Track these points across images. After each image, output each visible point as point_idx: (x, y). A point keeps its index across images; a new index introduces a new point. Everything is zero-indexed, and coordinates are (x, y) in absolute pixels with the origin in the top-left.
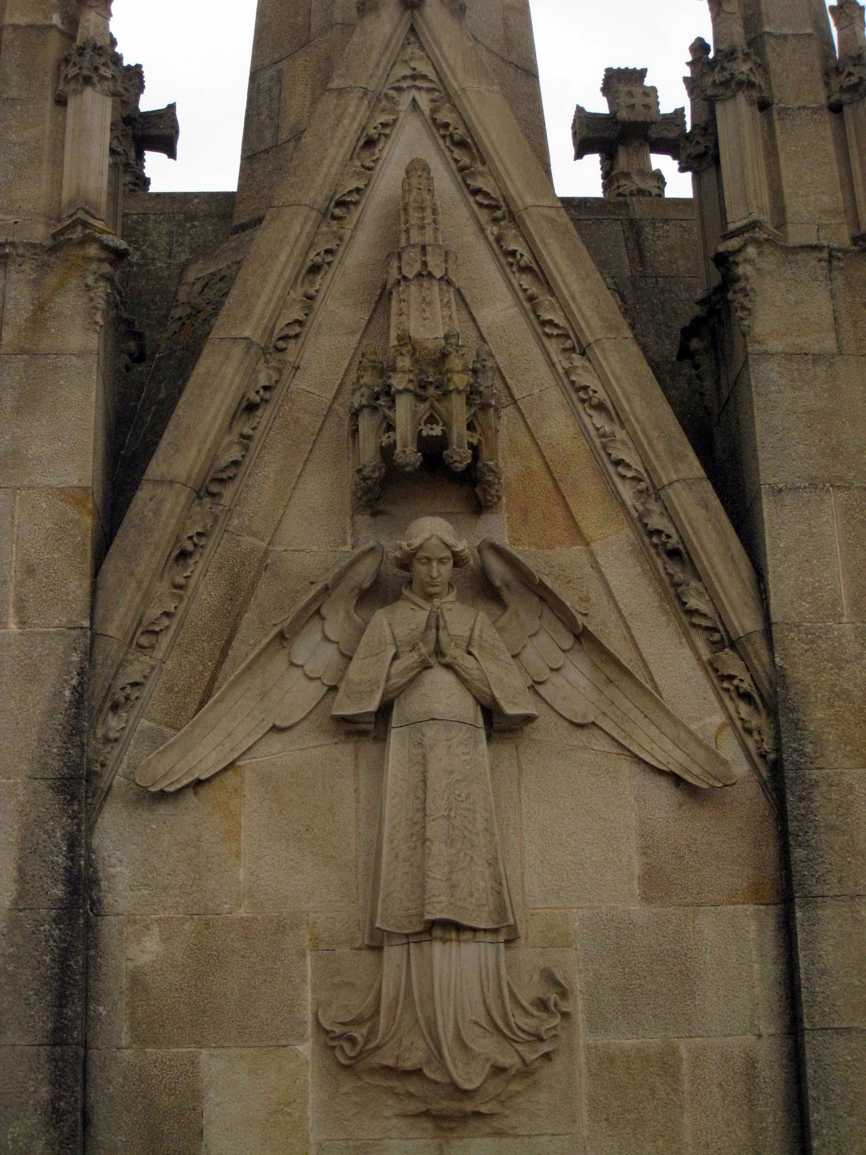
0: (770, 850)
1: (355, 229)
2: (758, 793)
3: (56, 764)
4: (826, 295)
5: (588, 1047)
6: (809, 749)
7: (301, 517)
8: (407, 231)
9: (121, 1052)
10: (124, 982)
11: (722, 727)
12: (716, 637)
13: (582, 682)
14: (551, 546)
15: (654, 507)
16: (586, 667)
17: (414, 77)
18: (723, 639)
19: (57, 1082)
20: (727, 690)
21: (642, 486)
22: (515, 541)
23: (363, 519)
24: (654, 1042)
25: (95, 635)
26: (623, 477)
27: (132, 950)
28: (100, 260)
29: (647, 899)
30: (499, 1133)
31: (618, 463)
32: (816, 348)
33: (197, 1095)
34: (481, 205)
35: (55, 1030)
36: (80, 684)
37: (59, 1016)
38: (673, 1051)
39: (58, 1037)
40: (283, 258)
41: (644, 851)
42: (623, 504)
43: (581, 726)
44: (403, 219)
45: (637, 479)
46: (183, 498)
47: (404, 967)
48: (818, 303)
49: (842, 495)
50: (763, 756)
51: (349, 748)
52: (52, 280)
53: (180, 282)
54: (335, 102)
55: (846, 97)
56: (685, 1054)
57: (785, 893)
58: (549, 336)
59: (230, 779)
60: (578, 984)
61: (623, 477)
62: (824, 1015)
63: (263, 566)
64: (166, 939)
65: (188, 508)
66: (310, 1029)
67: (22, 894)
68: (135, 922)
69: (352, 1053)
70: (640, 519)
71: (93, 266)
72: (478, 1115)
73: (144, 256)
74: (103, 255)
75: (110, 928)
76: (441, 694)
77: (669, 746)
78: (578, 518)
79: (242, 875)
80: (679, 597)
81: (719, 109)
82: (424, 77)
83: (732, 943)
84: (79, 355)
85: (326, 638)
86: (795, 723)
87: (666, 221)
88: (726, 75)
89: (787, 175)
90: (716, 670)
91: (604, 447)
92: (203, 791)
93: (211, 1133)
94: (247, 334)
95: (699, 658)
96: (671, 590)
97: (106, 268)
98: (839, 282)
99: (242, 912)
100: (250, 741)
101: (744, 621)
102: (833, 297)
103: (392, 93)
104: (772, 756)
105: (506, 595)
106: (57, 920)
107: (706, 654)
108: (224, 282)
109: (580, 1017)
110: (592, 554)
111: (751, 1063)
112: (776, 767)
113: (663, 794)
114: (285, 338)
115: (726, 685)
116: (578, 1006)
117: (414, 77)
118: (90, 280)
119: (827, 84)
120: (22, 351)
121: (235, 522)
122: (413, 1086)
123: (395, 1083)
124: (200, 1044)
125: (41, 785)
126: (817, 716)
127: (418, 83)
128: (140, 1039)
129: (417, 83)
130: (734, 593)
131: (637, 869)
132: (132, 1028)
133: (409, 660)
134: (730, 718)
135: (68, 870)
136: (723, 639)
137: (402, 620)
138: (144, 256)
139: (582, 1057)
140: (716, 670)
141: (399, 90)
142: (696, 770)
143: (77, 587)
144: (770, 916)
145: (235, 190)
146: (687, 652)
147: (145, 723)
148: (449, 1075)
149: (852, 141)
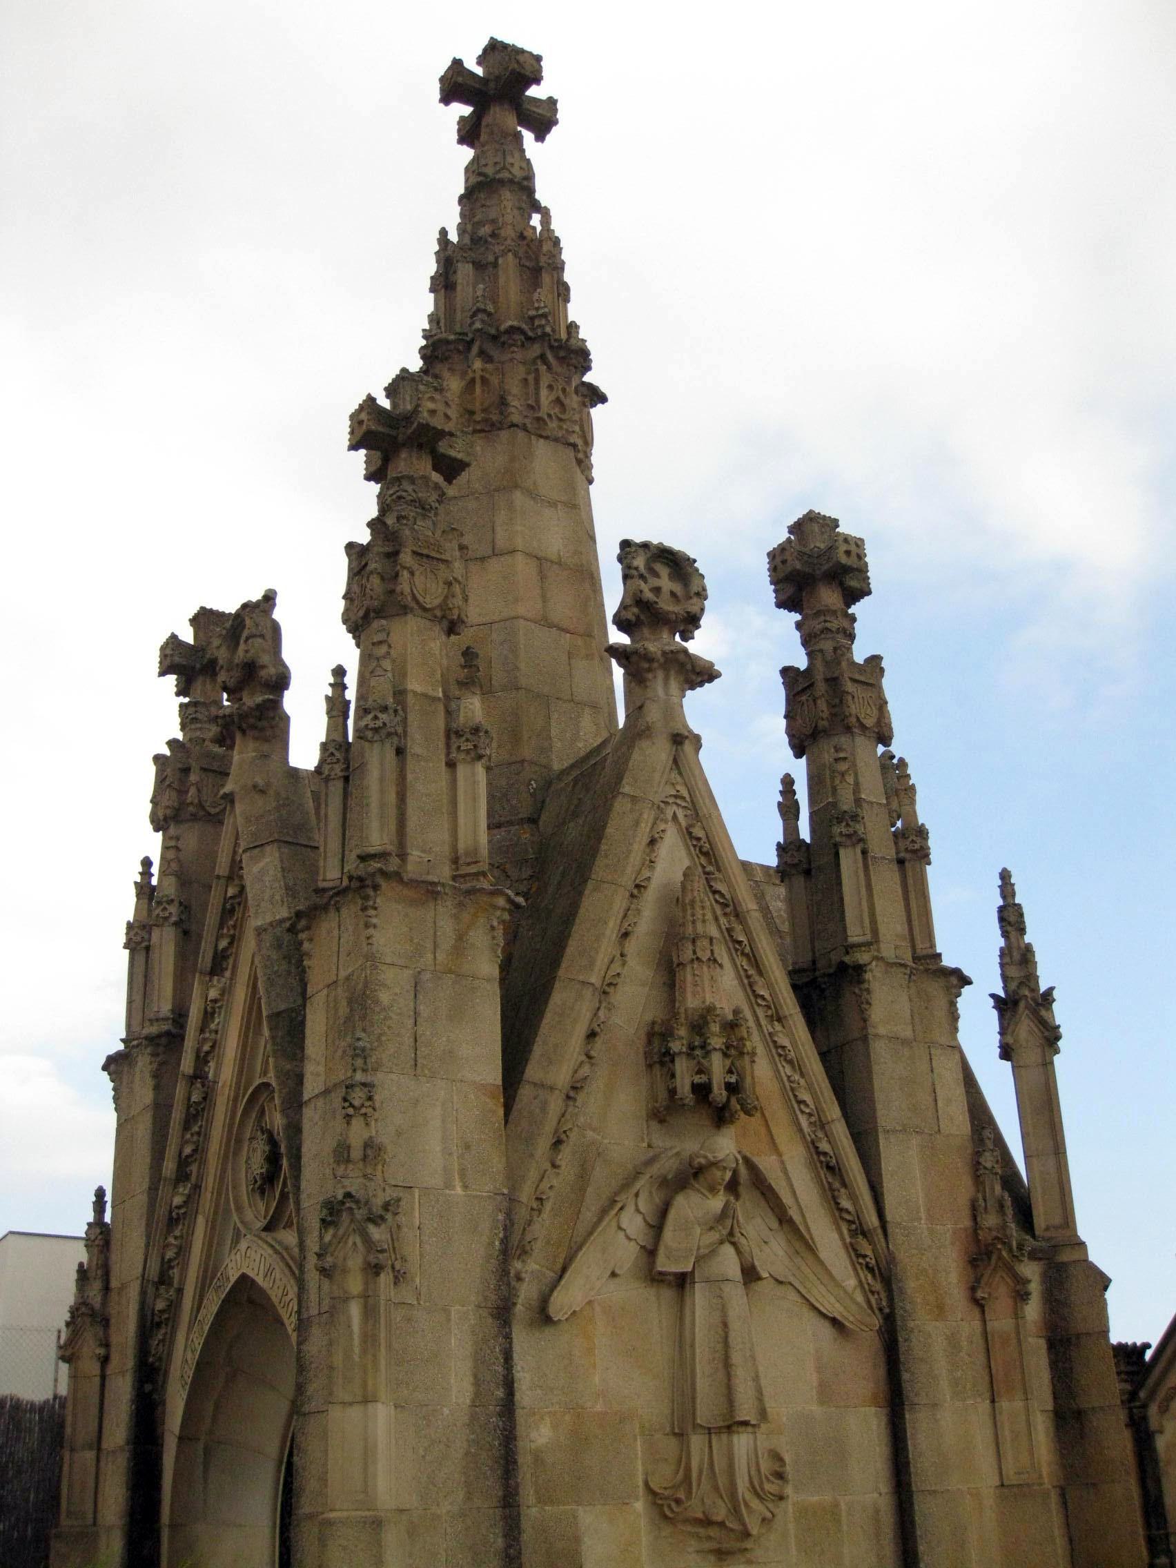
3: (493, 1297)
6: (908, 1307)
7: (615, 1120)
8: (694, 922)
9: (531, 1511)
10: (529, 1458)
12: (853, 1227)
13: (781, 1253)
15: (820, 1134)
16: (783, 1243)
17: (676, 797)
18: (859, 1230)
20: (860, 1264)
21: (813, 1119)
23: (654, 1124)
24: (828, 1498)
25: (512, 1200)
26: (802, 1112)
27: (534, 1435)
28: (504, 909)
29: (822, 1403)
30: (749, 1562)
31: (800, 1102)
32: (902, 1035)
33: (577, 1540)
34: (717, 901)
35: (505, 1497)
36: (506, 1237)
41: (819, 1369)
42: (801, 1130)
43: (781, 1283)
44: (689, 912)
45: (810, 1115)
47: (707, 1450)
50: (881, 1310)
51: (652, 1291)
52: (466, 916)
54: (629, 805)
55: (908, 856)
56: (843, 1507)
57: (895, 1401)
58: (759, 1005)
60: (787, 1458)
61: (802, 1112)
64: (555, 1427)
66: (641, 1490)
67: (477, 1394)
68: (534, 1414)
69: (666, 1507)
70: (813, 1142)
71: (498, 913)
74: (508, 907)
76: (728, 1263)
77: (832, 1300)
78: (776, 1137)
79: (597, 1379)
80: (834, 1198)
81: (842, 852)
82: (683, 798)
83: (866, 1429)
84: (488, 980)
86: (900, 1289)
88: (851, 830)
90: (855, 1250)
91: (792, 1089)
95: (842, 1239)
96: (829, 1193)
97: (506, 916)
101: (872, 1220)
103: (662, 805)
104: (887, 1311)
105: (742, 1189)
106: (500, 1415)
110: (782, 1162)
113: (826, 1330)
114: (610, 984)
115: (861, 1260)
117: (676, 797)
118: (495, 924)
119: (896, 843)
120: (450, 971)
121: (582, 1119)
122: (713, 1532)
123: (701, 1531)
124: (578, 1503)
125: (485, 1313)
127: (679, 801)
128: (541, 1501)
129: (679, 801)
132: (536, 1492)
133: (714, 1236)
134: (860, 1281)
136: (859, 1230)
140: (855, 1250)
141: (666, 803)
142: (851, 1319)
146: (836, 1236)
148: (744, 1525)
149: (911, 888)
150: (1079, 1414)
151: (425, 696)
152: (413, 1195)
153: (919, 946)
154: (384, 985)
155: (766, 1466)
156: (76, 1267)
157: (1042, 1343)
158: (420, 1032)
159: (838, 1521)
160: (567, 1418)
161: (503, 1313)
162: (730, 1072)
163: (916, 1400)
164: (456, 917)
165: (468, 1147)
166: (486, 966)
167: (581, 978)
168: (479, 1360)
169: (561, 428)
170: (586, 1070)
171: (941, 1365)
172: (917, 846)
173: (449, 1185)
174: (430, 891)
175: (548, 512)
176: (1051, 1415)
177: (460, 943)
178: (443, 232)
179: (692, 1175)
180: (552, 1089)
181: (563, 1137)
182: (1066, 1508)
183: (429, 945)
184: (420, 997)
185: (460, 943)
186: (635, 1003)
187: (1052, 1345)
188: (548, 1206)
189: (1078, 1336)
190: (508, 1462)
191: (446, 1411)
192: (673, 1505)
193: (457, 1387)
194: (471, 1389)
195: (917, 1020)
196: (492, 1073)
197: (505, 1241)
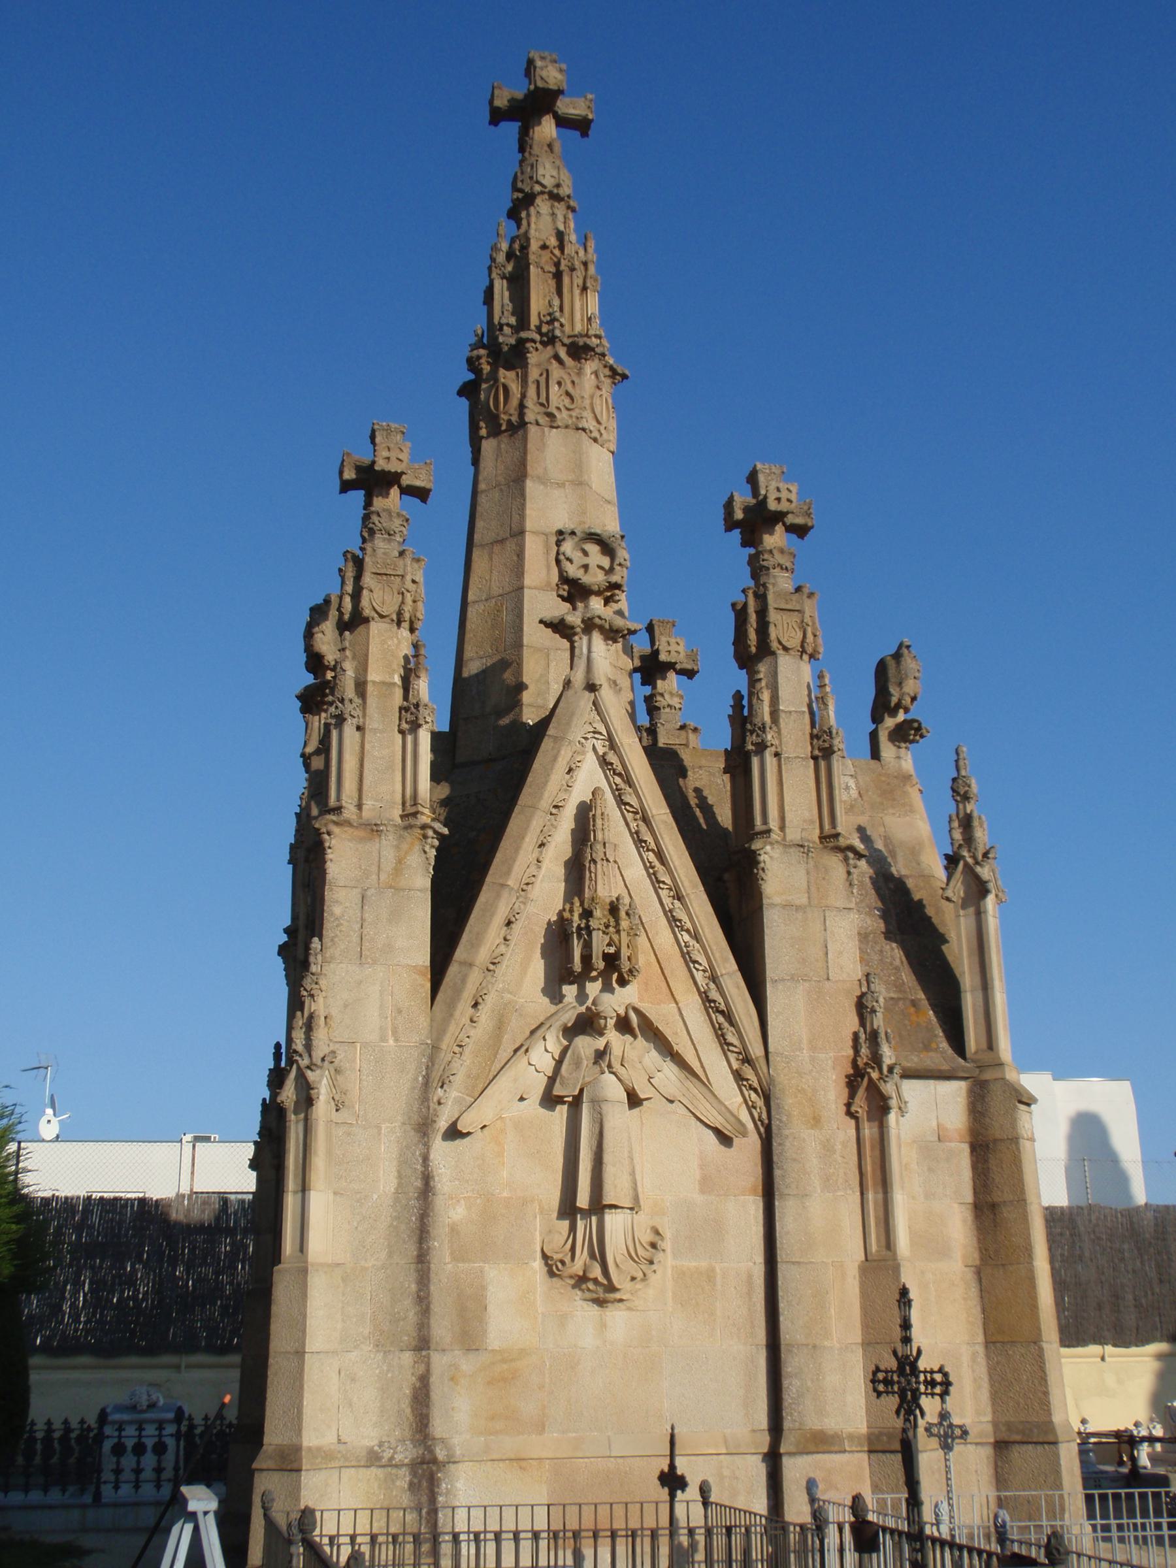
4: (804, 872)
5: (673, 1267)
6: (784, 1119)
11: (740, 1105)
13: (674, 1078)
14: (659, 1004)
15: (712, 986)
22: (641, 1000)
24: (704, 1264)
26: (697, 970)
27: (452, 1213)
29: (702, 1191)
30: (629, 1309)
32: (798, 902)
33: (483, 1288)
38: (713, 1270)
41: (702, 1167)
48: (799, 876)
49: (807, 984)
52: (405, 846)
56: (718, 1271)
60: (668, 1233)
61: (697, 970)
62: (787, 1254)
66: (539, 1255)
67: (400, 1185)
72: (621, 1300)
76: (612, 1089)
77: (716, 1114)
82: (600, 733)
84: (420, 891)
85: (547, 1051)
87: (700, 767)
93: (490, 1308)
99: (505, 1194)
101: (756, 1050)
102: (808, 873)
106: (418, 1199)
107: (735, 1065)
109: (669, 1250)
110: (679, 1009)
111: (750, 1276)
112: (768, 1128)
114: (527, 884)
116: (667, 1244)
117: (594, 732)
120: (391, 887)
125: (408, 1128)
128: (455, 1259)
130: (751, 1036)
131: (698, 1177)
132: (452, 1254)
137: (585, 1045)
139: (669, 1271)
141: (586, 739)
142: (730, 1128)
150: (993, 1207)
151: (384, 683)
153: (827, 826)
154: (337, 902)
155: (646, 1237)
156: (261, 1102)
157: (966, 1148)
158: (365, 932)
160: (478, 1201)
161: (424, 1127)
162: (609, 945)
163: (786, 1191)
164: (397, 847)
165: (400, 1012)
166: (420, 880)
167: (501, 881)
168: (403, 1162)
169: (571, 416)
170: (503, 949)
171: (813, 1162)
172: (827, 745)
173: (383, 1039)
174: (374, 829)
175: (557, 493)
176: (970, 1207)
177: (398, 870)
179: (588, 1024)
181: (480, 1000)
183: (374, 869)
185: (398, 870)
187: (974, 1148)
188: (467, 1050)
189: (995, 1141)
190: (422, 1232)
191: (375, 1196)
192: (559, 1265)
193: (385, 1179)
194: (396, 1181)
195: (813, 889)
196: (423, 957)
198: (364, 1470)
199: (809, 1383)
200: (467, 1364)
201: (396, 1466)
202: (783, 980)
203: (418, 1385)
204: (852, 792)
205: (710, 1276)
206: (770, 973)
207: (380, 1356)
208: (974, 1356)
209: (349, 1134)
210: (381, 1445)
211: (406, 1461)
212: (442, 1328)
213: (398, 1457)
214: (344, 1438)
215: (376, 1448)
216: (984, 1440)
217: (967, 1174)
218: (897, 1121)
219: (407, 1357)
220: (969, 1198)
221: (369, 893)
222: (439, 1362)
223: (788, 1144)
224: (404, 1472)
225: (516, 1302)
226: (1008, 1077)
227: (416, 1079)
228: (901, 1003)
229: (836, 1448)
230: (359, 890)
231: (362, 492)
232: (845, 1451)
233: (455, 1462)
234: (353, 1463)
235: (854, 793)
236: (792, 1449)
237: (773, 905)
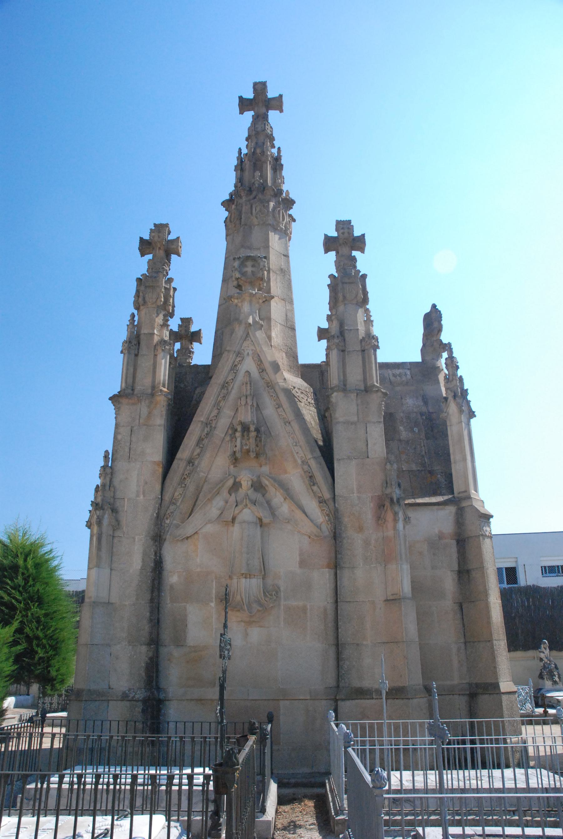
0: (333, 555)
1: (232, 389)
2: (441, 536)
9: (168, 605)
19: (151, 612)
24: (301, 604)
33: (186, 616)
37: (152, 596)
39: (152, 600)
40: (212, 398)
41: (301, 555)
46: (185, 464)
53: (194, 393)
56: (308, 607)
57: (336, 565)
59: (196, 536)
63: (205, 481)
65: (187, 466)
73: (185, 385)
75: (165, 573)
79: (198, 560)
83: (322, 579)
89: (348, 370)
92: (189, 540)
94: (202, 419)
98: (359, 401)
100: (201, 527)
102: (357, 405)
106: (152, 572)
108: (203, 393)
120: (145, 425)
125: (148, 538)
126: (346, 520)
131: (298, 559)
135: (154, 560)
138: (185, 385)
143: (158, 487)
144: (332, 572)
145: (210, 363)
147: (175, 522)
152: (124, 501)
157: (454, 542)
159: (306, 613)
164: (149, 407)
173: (138, 496)
176: (456, 572)
178: (240, 150)
180: (182, 460)
182: (158, 633)
183: (138, 417)
184: (133, 435)
186: (284, 407)
187: (458, 542)
191: (131, 571)
194: (141, 564)
197: (158, 514)
198: (120, 702)
199: (354, 663)
200: (176, 653)
201: (135, 701)
202: (344, 459)
203: (149, 661)
204: (408, 376)
205: (304, 609)
206: (336, 456)
207: (131, 647)
208: (459, 649)
209: (120, 541)
210: (130, 690)
211: (141, 698)
212: (166, 635)
213: (137, 696)
214: (112, 687)
215: (127, 692)
216: (463, 693)
217: (455, 556)
218: (404, 527)
219: (144, 649)
220: (456, 568)
221: (135, 428)
222: (163, 651)
223: (345, 541)
224: (140, 704)
225: (200, 624)
226: (474, 505)
227: (153, 514)
228: (423, 472)
229: (368, 697)
230: (130, 427)
231: (326, 340)
232: (373, 699)
233: (168, 700)
234: (115, 699)
235: (409, 377)
236: (343, 697)
237: (338, 423)
